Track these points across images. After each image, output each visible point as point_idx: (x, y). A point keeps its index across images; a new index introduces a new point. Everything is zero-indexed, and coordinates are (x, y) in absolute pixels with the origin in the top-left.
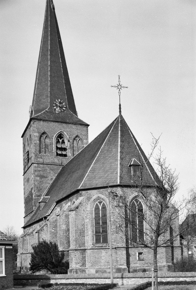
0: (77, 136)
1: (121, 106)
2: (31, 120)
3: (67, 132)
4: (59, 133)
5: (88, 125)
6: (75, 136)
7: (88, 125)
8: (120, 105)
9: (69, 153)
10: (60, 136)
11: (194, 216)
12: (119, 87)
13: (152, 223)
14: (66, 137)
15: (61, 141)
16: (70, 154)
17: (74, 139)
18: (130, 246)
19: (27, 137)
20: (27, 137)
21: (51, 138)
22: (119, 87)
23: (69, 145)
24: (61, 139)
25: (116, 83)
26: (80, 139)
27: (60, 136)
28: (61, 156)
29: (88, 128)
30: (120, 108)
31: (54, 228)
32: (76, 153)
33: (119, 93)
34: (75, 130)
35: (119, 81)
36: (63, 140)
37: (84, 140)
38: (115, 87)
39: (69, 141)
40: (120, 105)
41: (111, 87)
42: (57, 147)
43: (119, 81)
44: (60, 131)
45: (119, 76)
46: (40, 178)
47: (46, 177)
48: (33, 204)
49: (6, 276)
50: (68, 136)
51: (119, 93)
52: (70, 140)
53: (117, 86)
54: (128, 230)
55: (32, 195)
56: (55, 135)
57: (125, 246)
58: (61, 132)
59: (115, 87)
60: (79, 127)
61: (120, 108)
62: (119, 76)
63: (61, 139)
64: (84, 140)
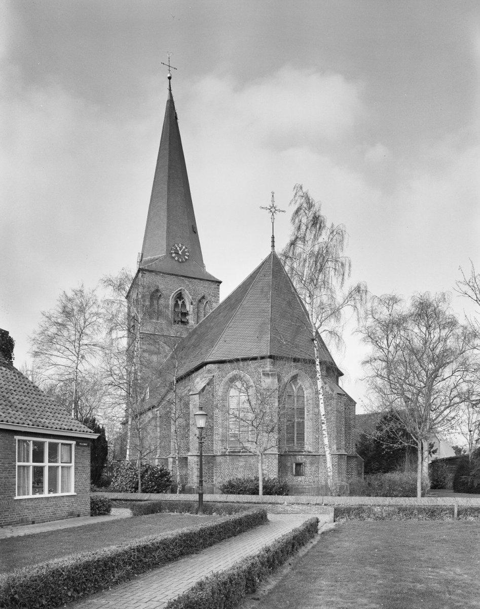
0: (203, 297)
1: (271, 244)
2: (139, 271)
3: (189, 290)
4: (177, 292)
5: (220, 282)
6: (200, 297)
7: (220, 282)
8: (273, 237)
9: (191, 319)
10: (180, 296)
12: (273, 210)
14: (188, 298)
15: (180, 303)
16: (193, 322)
17: (200, 301)
18: (203, 454)
21: (167, 298)
22: (273, 210)
24: (180, 300)
25: (268, 204)
26: (207, 302)
27: (180, 296)
29: (219, 286)
30: (273, 241)
32: (202, 319)
33: (273, 219)
34: (202, 289)
35: (273, 201)
36: (183, 302)
37: (214, 304)
39: (192, 304)
40: (273, 237)
41: (259, 209)
43: (273, 201)
44: (179, 289)
45: (273, 193)
49: (76, 494)
50: (191, 297)
51: (273, 219)
53: (270, 208)
54: (25, 490)
56: (173, 294)
58: (180, 290)
59: (266, 208)
60: (207, 284)
61: (273, 241)
62: (273, 193)
63: (180, 300)
64: (214, 304)
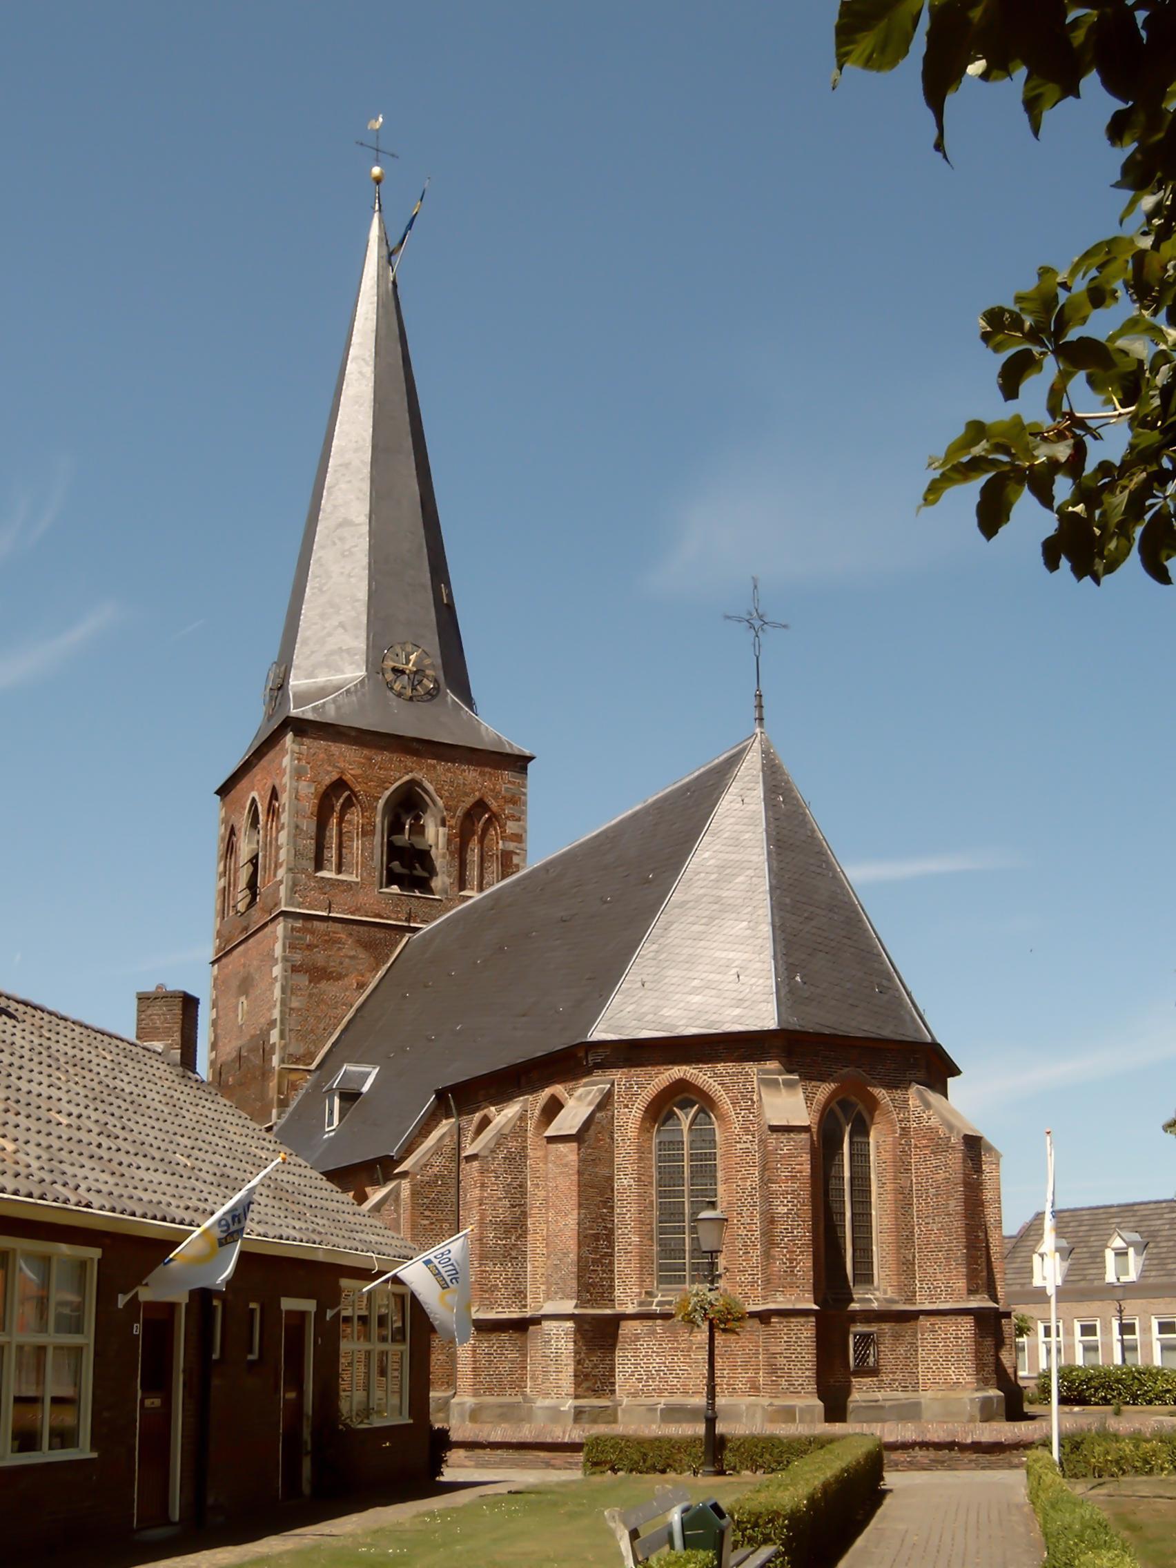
8: (424, 193)
11: (1175, 1431)
13: (566, 1215)
19: (254, 794)
20: (254, 794)
21: (369, 808)
23: (442, 841)
28: (1040, 1232)
31: (427, 1213)
33: (757, 646)
38: (740, 620)
40: (424, 193)
42: (390, 843)
46: (310, 982)
47: (340, 977)
48: (273, 1093)
51: (757, 646)
52: (448, 818)
53: (748, 617)
55: (266, 1053)
57: (702, 1336)
59: (740, 620)
